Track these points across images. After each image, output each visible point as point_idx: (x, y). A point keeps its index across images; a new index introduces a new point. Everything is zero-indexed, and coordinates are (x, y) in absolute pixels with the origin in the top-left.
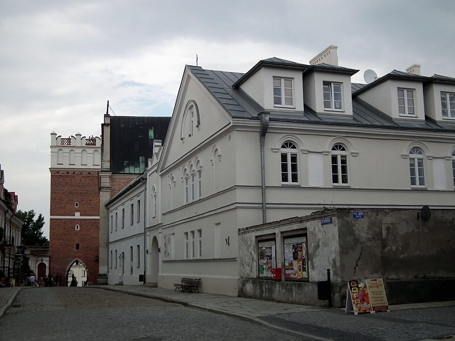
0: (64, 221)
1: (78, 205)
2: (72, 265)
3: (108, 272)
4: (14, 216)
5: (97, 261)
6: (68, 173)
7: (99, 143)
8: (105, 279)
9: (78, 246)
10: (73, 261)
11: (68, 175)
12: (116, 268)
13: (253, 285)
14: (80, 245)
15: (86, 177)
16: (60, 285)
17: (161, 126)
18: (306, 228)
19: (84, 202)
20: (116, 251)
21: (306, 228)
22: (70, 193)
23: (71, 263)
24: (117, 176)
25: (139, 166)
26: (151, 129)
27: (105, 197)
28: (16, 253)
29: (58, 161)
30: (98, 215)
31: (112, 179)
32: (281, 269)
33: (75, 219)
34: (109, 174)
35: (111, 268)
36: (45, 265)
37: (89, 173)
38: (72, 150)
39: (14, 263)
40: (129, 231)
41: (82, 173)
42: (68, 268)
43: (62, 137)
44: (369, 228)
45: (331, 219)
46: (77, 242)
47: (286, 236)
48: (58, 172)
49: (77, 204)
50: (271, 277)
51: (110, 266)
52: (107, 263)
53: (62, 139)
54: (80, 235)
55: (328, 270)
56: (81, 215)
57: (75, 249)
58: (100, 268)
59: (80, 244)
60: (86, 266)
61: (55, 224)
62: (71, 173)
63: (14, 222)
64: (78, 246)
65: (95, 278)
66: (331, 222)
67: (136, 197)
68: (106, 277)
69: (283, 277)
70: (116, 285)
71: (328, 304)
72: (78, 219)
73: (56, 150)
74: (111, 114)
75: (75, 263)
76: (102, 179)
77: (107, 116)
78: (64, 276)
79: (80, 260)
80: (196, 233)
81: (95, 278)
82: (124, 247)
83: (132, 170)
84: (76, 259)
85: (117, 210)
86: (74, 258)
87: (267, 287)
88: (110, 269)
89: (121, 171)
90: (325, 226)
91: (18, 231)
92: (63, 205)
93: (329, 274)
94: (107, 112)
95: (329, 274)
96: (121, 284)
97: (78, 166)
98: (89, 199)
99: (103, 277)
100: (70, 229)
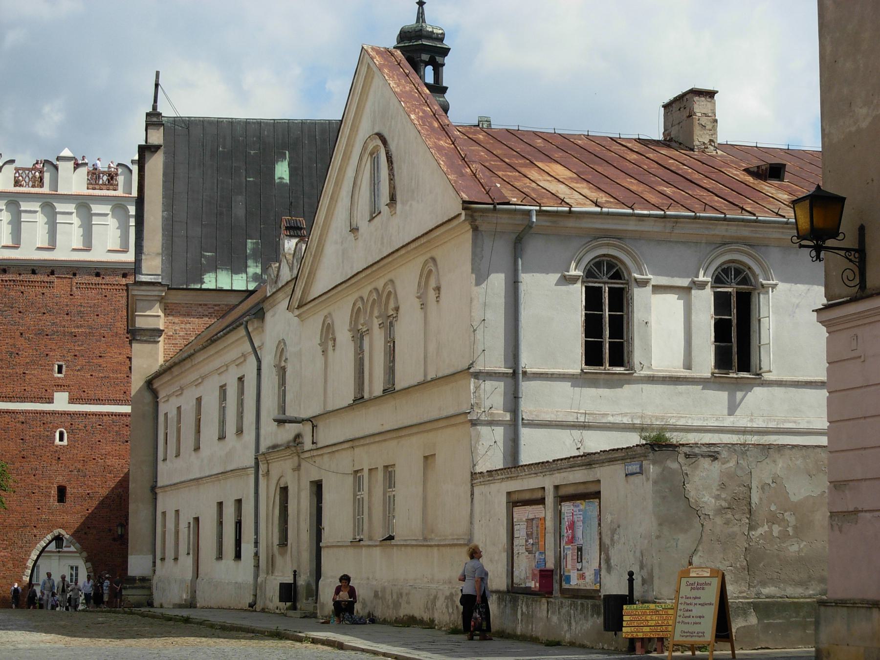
0: (22, 418)
3: (154, 571)
5: (123, 540)
7: (126, 187)
8: (145, 592)
10: (49, 537)
12: (176, 559)
13: (499, 604)
16: (17, 607)
17: (311, 144)
18: (599, 481)
19: (82, 361)
21: (599, 481)
22: (41, 333)
25: (246, 267)
32: (552, 571)
33: (54, 413)
35: (163, 559)
40: (213, 454)
43: (17, 164)
44: (723, 486)
45: (641, 467)
46: (60, 480)
47: (563, 497)
50: (530, 588)
53: (17, 170)
55: (631, 574)
56: (72, 401)
57: (53, 501)
58: (129, 557)
59: (68, 489)
60: (85, 554)
66: (641, 473)
69: (556, 587)
70: (180, 606)
74: (166, 111)
77: (153, 119)
82: (200, 504)
84: (56, 532)
87: (524, 610)
88: (158, 562)
89: (194, 282)
90: (631, 478)
92: (20, 370)
93: (631, 581)
94: (155, 107)
95: (631, 581)
96: (191, 604)
98: (97, 353)
99: (138, 584)
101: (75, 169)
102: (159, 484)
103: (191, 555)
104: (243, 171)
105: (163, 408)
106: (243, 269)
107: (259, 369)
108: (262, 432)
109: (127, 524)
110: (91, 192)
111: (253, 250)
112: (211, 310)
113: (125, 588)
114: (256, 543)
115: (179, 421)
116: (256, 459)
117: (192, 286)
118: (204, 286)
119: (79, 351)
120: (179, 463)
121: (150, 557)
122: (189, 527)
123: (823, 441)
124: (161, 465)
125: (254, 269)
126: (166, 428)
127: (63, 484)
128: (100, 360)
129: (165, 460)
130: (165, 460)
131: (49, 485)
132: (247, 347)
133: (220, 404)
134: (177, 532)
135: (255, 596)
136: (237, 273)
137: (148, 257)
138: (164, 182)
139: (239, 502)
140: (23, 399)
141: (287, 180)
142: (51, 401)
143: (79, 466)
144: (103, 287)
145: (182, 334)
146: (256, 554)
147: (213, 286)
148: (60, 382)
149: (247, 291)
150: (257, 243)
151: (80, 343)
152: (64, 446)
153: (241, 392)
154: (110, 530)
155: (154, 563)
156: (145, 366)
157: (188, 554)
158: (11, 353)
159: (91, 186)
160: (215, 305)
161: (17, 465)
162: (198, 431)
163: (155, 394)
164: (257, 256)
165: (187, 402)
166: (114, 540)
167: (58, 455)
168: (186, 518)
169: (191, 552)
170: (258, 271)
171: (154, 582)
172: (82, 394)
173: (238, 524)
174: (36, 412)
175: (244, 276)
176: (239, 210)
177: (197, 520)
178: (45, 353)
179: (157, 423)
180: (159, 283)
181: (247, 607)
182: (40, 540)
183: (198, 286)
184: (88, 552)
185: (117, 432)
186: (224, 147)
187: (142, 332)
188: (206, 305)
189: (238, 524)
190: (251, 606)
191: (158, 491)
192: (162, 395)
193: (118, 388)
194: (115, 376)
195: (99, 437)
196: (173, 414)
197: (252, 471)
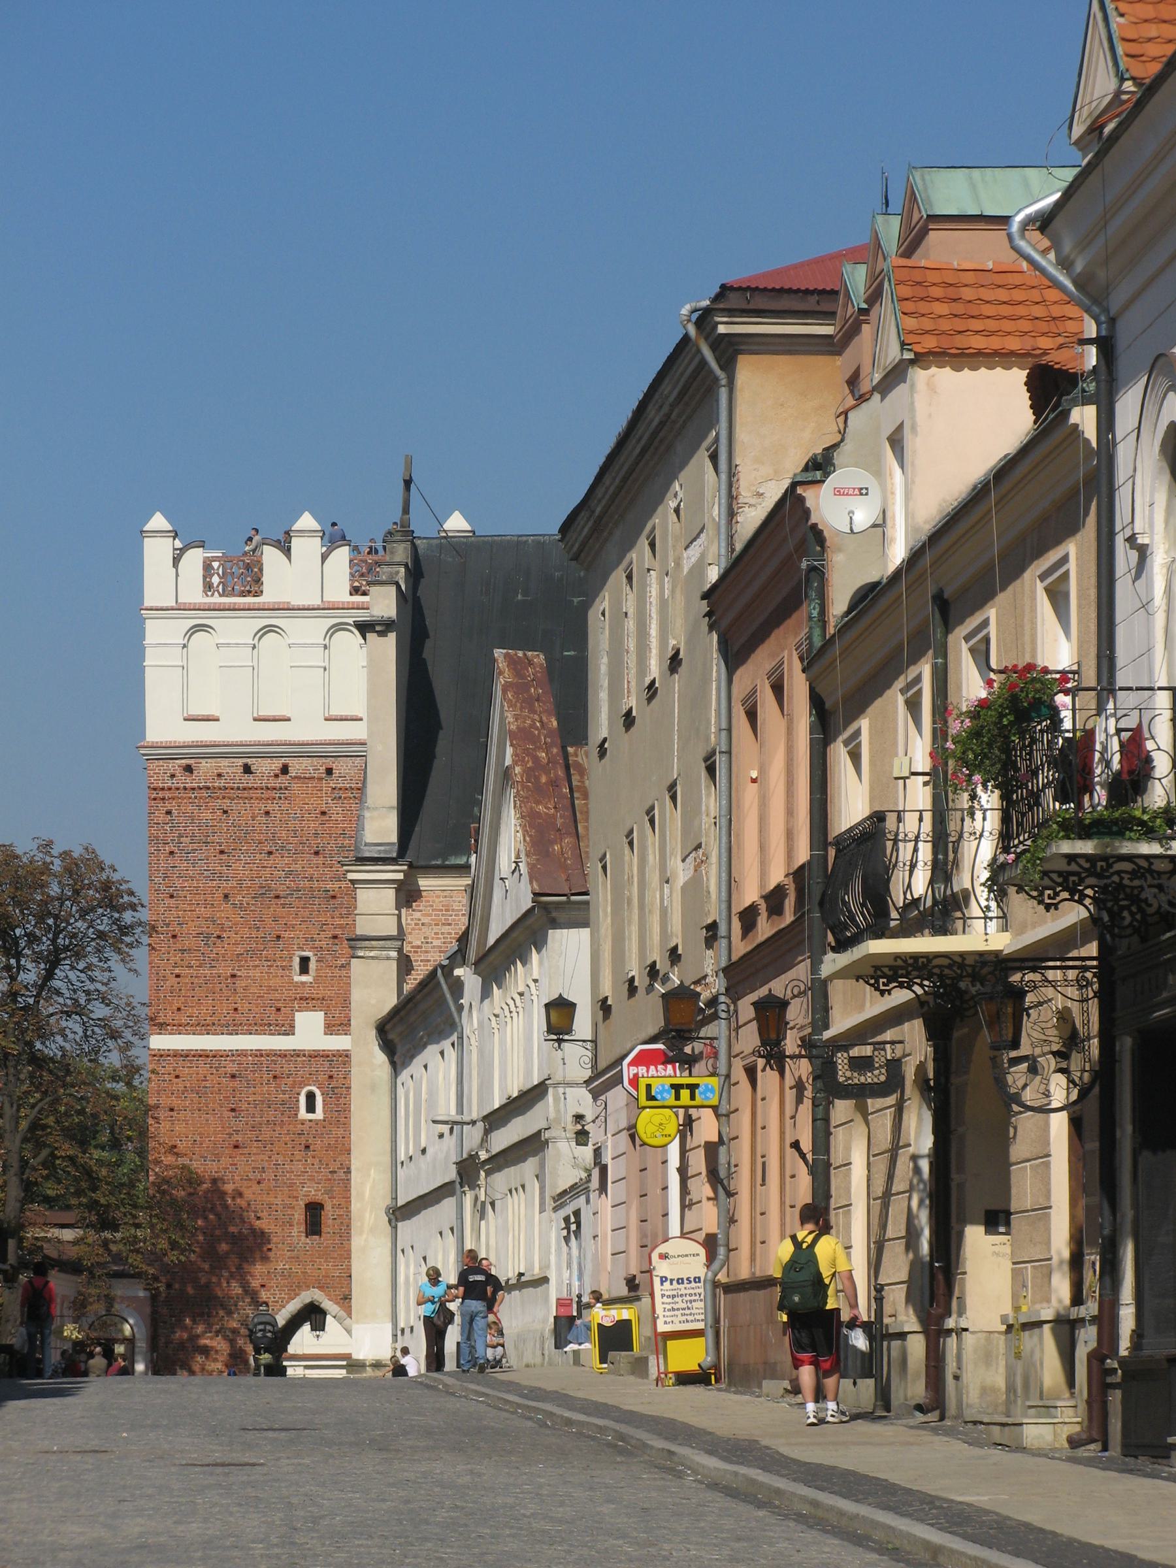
0: (232, 1068)
1: (312, 965)
6: (247, 769)
11: (248, 780)
22: (267, 894)
29: (185, 701)
31: (407, 895)
33: (297, 1054)
38: (269, 629)
41: (329, 771)
46: (313, 1192)
48: (189, 769)
49: (305, 961)
52: (388, 1309)
57: (298, 1229)
59: (328, 1207)
61: (179, 1085)
62: (265, 768)
71: (1100, 1448)
72: (315, 1055)
79: (327, 1304)
80: (520, 1189)
84: (305, 1297)
100: (271, 1115)
101: (287, 552)
119: (341, 927)
123: (1095, 963)
127: (319, 1197)
137: (375, 813)
140: (233, 1029)
142: (290, 1031)
145: (436, 943)
152: (317, 1122)
156: (373, 1002)
174: (259, 1054)
178: (274, 933)
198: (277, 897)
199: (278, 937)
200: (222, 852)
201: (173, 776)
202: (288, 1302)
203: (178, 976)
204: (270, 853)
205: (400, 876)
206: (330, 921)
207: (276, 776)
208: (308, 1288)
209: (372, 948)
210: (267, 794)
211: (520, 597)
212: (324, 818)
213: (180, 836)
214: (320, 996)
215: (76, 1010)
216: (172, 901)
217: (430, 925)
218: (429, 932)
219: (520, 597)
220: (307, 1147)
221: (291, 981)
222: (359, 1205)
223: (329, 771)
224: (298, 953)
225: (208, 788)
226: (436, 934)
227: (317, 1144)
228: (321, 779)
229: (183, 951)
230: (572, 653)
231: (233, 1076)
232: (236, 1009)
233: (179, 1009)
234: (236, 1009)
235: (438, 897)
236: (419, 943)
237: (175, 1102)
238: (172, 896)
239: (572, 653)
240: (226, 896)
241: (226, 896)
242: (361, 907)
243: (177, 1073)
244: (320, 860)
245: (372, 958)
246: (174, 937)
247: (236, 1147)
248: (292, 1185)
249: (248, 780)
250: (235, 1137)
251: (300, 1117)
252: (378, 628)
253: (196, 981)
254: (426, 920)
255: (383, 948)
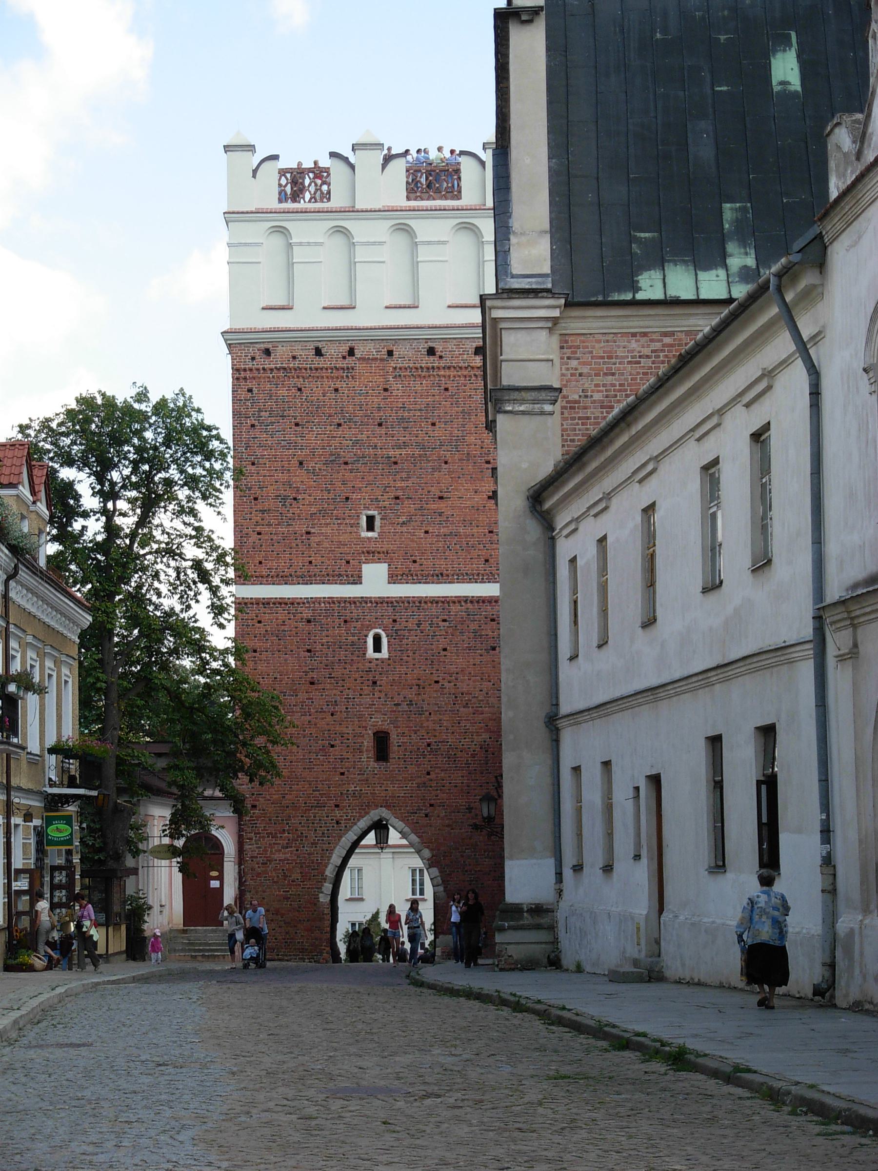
0: (307, 614)
1: (377, 523)
2: (355, 844)
3: (560, 892)
4: (24, 574)
5: (491, 828)
6: (318, 352)
9: (382, 742)
10: (363, 824)
11: (320, 362)
12: (608, 869)
14: (394, 738)
15: (417, 372)
19: (409, 507)
20: (607, 764)
22: (336, 461)
23: (351, 836)
24: (590, 323)
26: (786, 43)
27: (527, 448)
28: (52, 784)
30: (490, 578)
33: (364, 600)
34: (547, 309)
35: (578, 868)
36: (217, 846)
37: (431, 351)
39: (40, 834)
40: (690, 629)
41: (390, 353)
42: (336, 859)
43: (282, 164)
46: (379, 722)
48: (267, 352)
49: (371, 520)
51: (569, 860)
53: (282, 172)
54: (393, 683)
56: (394, 578)
57: (367, 759)
60: (427, 853)
61: (261, 629)
62: (333, 352)
63: (23, 603)
64: (382, 742)
65: (478, 911)
67: (739, 409)
68: (545, 920)
73: (256, 231)
75: (372, 835)
76: (508, 339)
78: (315, 902)
81: (478, 911)
82: (670, 744)
83: (680, 282)
84: (375, 815)
85: (599, 530)
86: (364, 810)
88: (567, 873)
89: (619, 290)
91: (57, 663)
92: (300, 527)
97: (371, 315)
99: (527, 919)
102: (564, 709)
103: (644, 860)
104: (706, 74)
105: (565, 549)
106: (720, 259)
107: (815, 393)
108: (832, 548)
109: (500, 796)
110: (413, 203)
111: (738, 223)
112: (658, 345)
113: (502, 929)
114: (826, 832)
115: (603, 569)
116: (818, 619)
117: (616, 297)
118: (640, 296)
119: (402, 488)
120: (607, 660)
121: (551, 862)
122: (637, 797)
124: (565, 669)
125: (740, 258)
126: (575, 591)
127: (385, 727)
128: (442, 505)
129: (573, 658)
130: (573, 658)
131: (358, 730)
132: (782, 345)
133: (705, 508)
134: (608, 808)
135: (831, 966)
136: (707, 268)
137: (524, 239)
138: (550, 103)
139: (767, 733)
141: (796, 83)
142: (357, 580)
143: (411, 694)
144: (442, 373)
145: (597, 396)
146: (828, 861)
147: (658, 295)
148: (372, 547)
149: (730, 301)
150: (743, 210)
151: (404, 475)
152: (382, 660)
153: (763, 466)
154: (470, 809)
155: (559, 875)
156: (524, 465)
157: (637, 857)
158: (285, 498)
159: (412, 196)
160: (665, 334)
161: (302, 696)
162: (650, 583)
163: (547, 521)
164: (745, 233)
165: (621, 524)
166: (475, 827)
167: (373, 678)
168: (629, 776)
169: (644, 853)
170: (751, 261)
171: (560, 915)
172: (413, 567)
173: (768, 786)
174: (331, 601)
175: (722, 273)
176: (703, 148)
177: (655, 780)
179: (554, 583)
180: (548, 291)
181: (809, 992)
182: (347, 829)
183: (628, 296)
184: (431, 850)
185: (475, 632)
186: (665, 31)
187: (515, 395)
188: (645, 334)
189: (768, 786)
190: (818, 991)
191: (561, 724)
192: (561, 520)
193: (475, 553)
194: (468, 531)
195: (443, 642)
196: (588, 554)
197: (809, 650)
198: (346, 463)
199: (347, 498)
200: (297, 425)
201: (253, 359)
202: (358, 820)
203: (259, 534)
204: (339, 425)
205: (556, 313)
206: (392, 483)
207: (344, 358)
208: (376, 807)
209: (523, 401)
210: (336, 373)
211: (658, 36)
212: (386, 394)
213: (260, 411)
214: (384, 550)
215: (171, 552)
216: (253, 468)
217: (589, 375)
218: (587, 384)
219: (658, 36)
220: (375, 683)
221: (359, 537)
222: (511, 714)
223: (390, 353)
224: (364, 512)
225: (285, 369)
226: (597, 385)
227: (383, 680)
228: (382, 360)
229: (263, 511)
230: (724, 88)
231: (309, 621)
232: (310, 562)
233: (260, 563)
234: (310, 562)
235: (599, 341)
236: (576, 397)
237: (258, 645)
238: (253, 464)
239: (724, 88)
240: (301, 463)
241: (301, 463)
242: (508, 352)
243: (259, 619)
244: (383, 431)
245: (523, 413)
246: (256, 499)
247: (312, 683)
248: (360, 717)
249: (320, 362)
250: (311, 674)
251: (368, 656)
252: (524, 18)
253: (275, 538)
254: (585, 370)
255: (535, 401)
